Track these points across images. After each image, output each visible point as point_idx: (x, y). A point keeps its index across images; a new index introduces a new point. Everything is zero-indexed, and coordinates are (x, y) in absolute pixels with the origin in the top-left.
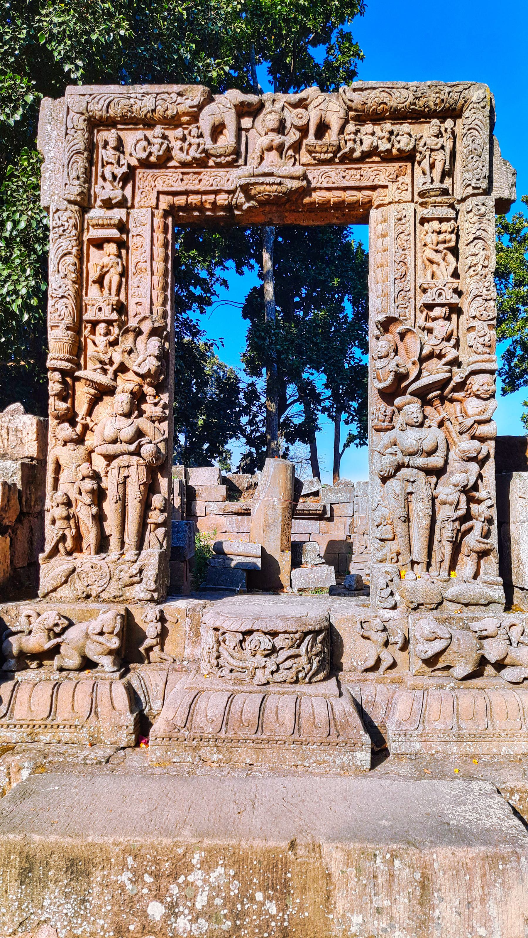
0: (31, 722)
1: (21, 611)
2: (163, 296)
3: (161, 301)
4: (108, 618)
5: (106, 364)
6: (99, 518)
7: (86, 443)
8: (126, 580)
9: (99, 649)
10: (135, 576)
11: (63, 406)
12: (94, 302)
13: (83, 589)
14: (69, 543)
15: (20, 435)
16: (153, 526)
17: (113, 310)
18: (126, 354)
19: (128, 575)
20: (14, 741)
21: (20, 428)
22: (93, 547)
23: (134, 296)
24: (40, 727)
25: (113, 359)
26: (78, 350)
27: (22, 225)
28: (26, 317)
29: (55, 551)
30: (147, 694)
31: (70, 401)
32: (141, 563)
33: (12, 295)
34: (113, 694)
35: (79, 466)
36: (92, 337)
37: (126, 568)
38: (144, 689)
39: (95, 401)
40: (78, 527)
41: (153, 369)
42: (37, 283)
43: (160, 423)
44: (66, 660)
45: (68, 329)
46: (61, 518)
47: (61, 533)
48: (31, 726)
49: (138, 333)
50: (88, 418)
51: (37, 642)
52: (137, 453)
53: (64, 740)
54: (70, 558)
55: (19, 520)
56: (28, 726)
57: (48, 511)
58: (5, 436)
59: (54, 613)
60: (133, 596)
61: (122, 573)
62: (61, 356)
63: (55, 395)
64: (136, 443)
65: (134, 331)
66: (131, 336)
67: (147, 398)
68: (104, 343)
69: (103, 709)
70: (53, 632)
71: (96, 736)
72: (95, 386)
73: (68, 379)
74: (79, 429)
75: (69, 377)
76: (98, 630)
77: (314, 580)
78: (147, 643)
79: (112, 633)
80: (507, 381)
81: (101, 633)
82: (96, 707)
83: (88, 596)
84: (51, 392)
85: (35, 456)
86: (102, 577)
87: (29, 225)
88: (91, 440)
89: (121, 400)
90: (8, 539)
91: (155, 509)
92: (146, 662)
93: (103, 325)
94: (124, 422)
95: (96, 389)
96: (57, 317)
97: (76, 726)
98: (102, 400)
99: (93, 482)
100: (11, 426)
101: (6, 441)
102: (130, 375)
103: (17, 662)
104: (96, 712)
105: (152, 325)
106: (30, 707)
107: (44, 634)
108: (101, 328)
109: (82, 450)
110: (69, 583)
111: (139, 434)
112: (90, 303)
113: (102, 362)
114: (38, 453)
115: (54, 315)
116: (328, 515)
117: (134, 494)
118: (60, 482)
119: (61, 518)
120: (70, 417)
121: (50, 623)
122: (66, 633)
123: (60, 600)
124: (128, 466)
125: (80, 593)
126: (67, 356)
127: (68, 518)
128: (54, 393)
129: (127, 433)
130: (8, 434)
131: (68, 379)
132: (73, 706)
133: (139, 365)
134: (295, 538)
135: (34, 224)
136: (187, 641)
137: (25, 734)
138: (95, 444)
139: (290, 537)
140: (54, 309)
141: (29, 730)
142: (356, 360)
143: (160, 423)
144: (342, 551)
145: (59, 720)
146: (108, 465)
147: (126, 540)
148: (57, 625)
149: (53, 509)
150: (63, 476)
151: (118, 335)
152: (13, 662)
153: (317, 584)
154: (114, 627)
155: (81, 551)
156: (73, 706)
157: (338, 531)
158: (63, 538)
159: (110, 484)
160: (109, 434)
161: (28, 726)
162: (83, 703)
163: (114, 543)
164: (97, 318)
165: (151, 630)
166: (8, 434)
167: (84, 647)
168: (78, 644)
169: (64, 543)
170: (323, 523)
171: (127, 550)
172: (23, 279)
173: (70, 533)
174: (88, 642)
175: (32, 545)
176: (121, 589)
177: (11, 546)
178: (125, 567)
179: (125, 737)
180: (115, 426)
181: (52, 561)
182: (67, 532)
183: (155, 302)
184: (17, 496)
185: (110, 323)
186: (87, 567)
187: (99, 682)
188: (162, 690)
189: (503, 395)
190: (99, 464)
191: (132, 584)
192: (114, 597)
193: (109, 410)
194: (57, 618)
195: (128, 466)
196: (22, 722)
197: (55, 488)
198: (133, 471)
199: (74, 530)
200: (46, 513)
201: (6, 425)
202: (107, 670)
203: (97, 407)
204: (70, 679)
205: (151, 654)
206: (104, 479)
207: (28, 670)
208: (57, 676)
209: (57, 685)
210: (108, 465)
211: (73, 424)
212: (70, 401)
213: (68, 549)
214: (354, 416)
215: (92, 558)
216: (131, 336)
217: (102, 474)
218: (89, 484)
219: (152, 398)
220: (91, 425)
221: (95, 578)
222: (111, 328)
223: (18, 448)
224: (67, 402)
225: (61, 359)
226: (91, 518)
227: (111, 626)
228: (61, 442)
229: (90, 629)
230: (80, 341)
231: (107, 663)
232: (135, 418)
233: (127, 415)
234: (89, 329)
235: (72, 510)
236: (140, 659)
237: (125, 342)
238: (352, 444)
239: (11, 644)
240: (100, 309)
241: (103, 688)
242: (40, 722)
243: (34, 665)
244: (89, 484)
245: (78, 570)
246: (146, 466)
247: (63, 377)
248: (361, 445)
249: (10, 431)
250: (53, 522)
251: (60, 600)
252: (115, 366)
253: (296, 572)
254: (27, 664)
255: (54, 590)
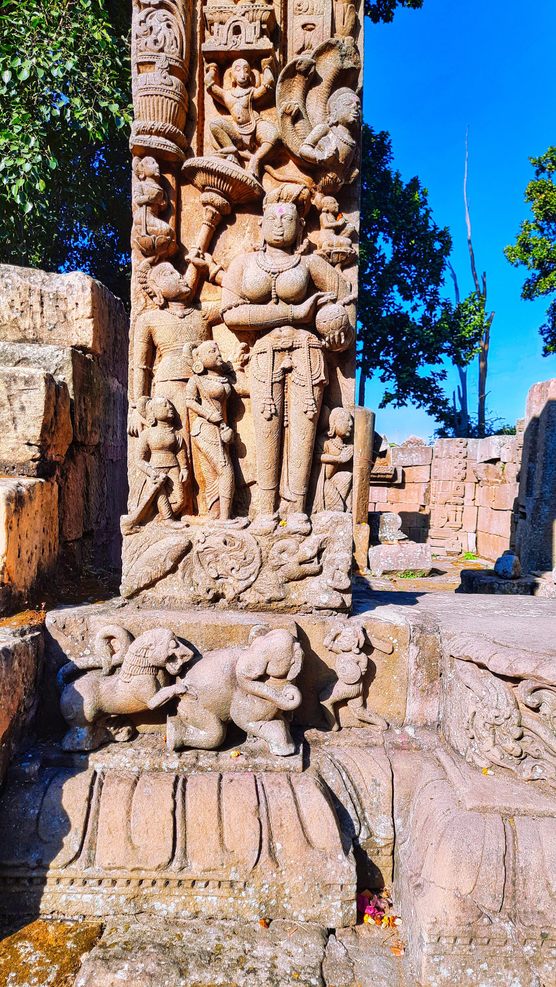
0: (134, 874)
1: (92, 627)
2: (352, 17)
3: (349, 26)
4: (274, 645)
5: (243, 148)
6: (234, 450)
7: (204, 305)
8: (292, 566)
9: (259, 708)
10: (309, 561)
11: (163, 226)
12: (223, 17)
13: (208, 583)
14: (177, 496)
15: (62, 307)
16: (329, 468)
17: (263, 33)
18: (288, 120)
19: (296, 559)
20: (99, 913)
21: (63, 293)
22: (224, 505)
23: (299, 11)
24: (154, 883)
25: (260, 134)
26: (188, 120)
27: (24, 76)
28: (29, 207)
29: (150, 511)
30: (358, 803)
31: (172, 219)
32: (321, 537)
33: (11, 174)
34: (303, 808)
35: (195, 347)
36: (216, 88)
37: (293, 547)
38: (351, 790)
39: (221, 222)
40: (190, 467)
41: (344, 150)
42: (44, 158)
43: (343, 268)
44: (191, 729)
45: (172, 70)
46: (162, 448)
47: (163, 475)
48: (134, 883)
49: (312, 80)
50: (207, 255)
51: (130, 690)
52: (308, 323)
53: (205, 911)
54: (178, 524)
55: (70, 455)
56: (129, 882)
57: (135, 435)
58: (37, 307)
59: (166, 635)
60: (302, 599)
61: (285, 555)
62: (159, 125)
63: (147, 204)
64: (309, 302)
65: (305, 73)
66: (298, 83)
67: (323, 216)
68: (244, 100)
69: (287, 845)
70: (164, 675)
71: (273, 902)
72: (226, 187)
73: (169, 177)
74: (190, 274)
75: (175, 170)
76: (258, 672)
77: (404, 560)
78: (340, 690)
79: (284, 676)
80: (549, 340)
81: (263, 678)
82: (270, 839)
83: (217, 598)
84: (136, 198)
85: (90, 345)
86: (245, 563)
87: (33, 78)
88: (211, 300)
89: (278, 215)
90: (56, 487)
91: (334, 437)
92: (335, 727)
93: (241, 63)
94: (279, 259)
95: (224, 194)
96: (150, 44)
97: (232, 884)
98: (232, 221)
99: (222, 379)
100: (45, 289)
101: (38, 316)
102: (290, 169)
103: (91, 733)
104: (271, 851)
105: (339, 64)
106: (129, 839)
107: (147, 678)
108: (238, 69)
109: (196, 319)
110: (179, 573)
111: (311, 286)
112: (217, 17)
113: (236, 141)
114: (95, 339)
115: (144, 40)
116: (399, 481)
117: (301, 402)
118: (154, 380)
119: (162, 448)
120: (171, 252)
121: (159, 654)
122: (189, 674)
123: (164, 604)
124: (291, 349)
125: (201, 591)
126: (170, 126)
127: (173, 448)
128: (145, 198)
129: (291, 280)
130: (42, 304)
131: (169, 177)
132: (221, 835)
133: (315, 144)
134: (371, 509)
135: (41, 73)
136: (411, 689)
137: (122, 899)
138: (223, 306)
139: (366, 506)
140: (144, 27)
141: (131, 889)
142: (396, 307)
143: (343, 268)
144: (415, 524)
145: (195, 869)
146: (246, 350)
147: (285, 491)
148: (172, 658)
149: (144, 428)
150: (161, 369)
151: (273, 84)
152: (84, 732)
153: (408, 565)
154: (290, 665)
155: (195, 512)
156: (221, 835)
157: (410, 500)
158: (166, 487)
159: (255, 382)
160: (254, 280)
161: (129, 882)
162: (242, 833)
163: (259, 497)
164: (230, 47)
165: (346, 668)
166: (42, 304)
167: (228, 703)
168: (216, 697)
169: (168, 495)
170: (392, 490)
171: (285, 512)
172: (26, 150)
173: (178, 477)
174: (237, 695)
175: (88, 501)
176: (281, 586)
177: (59, 500)
178: (290, 543)
179: (337, 908)
180: (268, 267)
181: (146, 529)
182: (173, 475)
183: (339, 25)
184: (68, 408)
185: (254, 58)
186: (215, 541)
187: (265, 779)
188: (388, 794)
189: (544, 356)
190: (229, 346)
191: (303, 577)
192: (270, 601)
193: (247, 241)
194: (173, 644)
195: (291, 349)
196: (115, 874)
197: (147, 390)
198: (299, 359)
199: (184, 473)
200: (130, 439)
201: (38, 288)
202: (275, 751)
203: (223, 235)
204: (202, 769)
205: (342, 711)
206: (239, 375)
207: (111, 746)
208: (173, 762)
209: (180, 784)
210: (246, 350)
211: (180, 265)
212: (172, 219)
213: (174, 507)
214: (391, 373)
215: (222, 526)
216: (298, 83)
217: (236, 367)
218: (215, 384)
219: (331, 217)
220: (213, 269)
221: (232, 563)
222: (255, 72)
223: (60, 330)
224: (167, 222)
225: (158, 133)
226: (220, 449)
227: (284, 663)
228: (159, 300)
229: (240, 669)
230: (191, 103)
231: (273, 737)
232: (302, 254)
233: (288, 247)
234: (212, 72)
235: (182, 434)
236: (326, 722)
237: (287, 97)
238: (389, 405)
239: (80, 699)
240: (237, 31)
241: (279, 798)
242: (154, 875)
243: (122, 734)
244: (215, 384)
245: (197, 548)
246: (323, 349)
247: (163, 169)
248: (400, 405)
249: (46, 299)
250: (147, 455)
251: (164, 604)
252: (261, 151)
253: (374, 550)
254: (109, 733)
255: (151, 584)
